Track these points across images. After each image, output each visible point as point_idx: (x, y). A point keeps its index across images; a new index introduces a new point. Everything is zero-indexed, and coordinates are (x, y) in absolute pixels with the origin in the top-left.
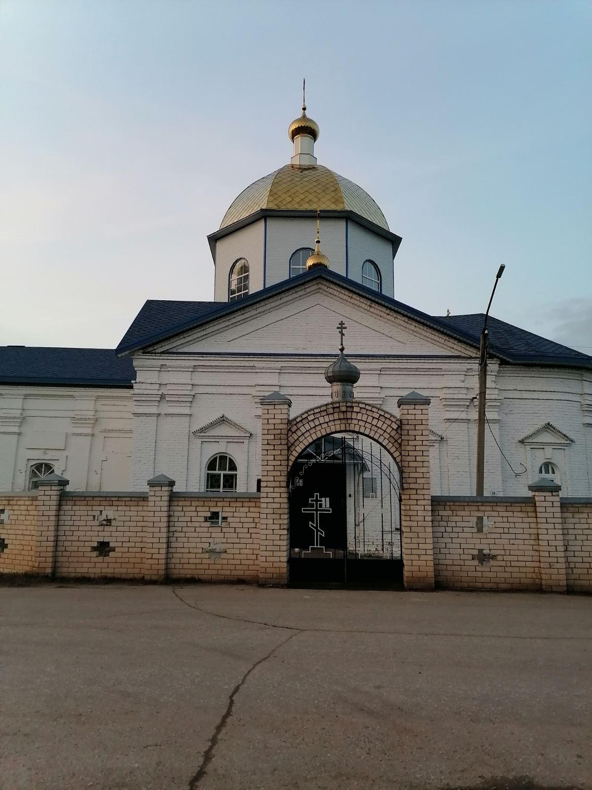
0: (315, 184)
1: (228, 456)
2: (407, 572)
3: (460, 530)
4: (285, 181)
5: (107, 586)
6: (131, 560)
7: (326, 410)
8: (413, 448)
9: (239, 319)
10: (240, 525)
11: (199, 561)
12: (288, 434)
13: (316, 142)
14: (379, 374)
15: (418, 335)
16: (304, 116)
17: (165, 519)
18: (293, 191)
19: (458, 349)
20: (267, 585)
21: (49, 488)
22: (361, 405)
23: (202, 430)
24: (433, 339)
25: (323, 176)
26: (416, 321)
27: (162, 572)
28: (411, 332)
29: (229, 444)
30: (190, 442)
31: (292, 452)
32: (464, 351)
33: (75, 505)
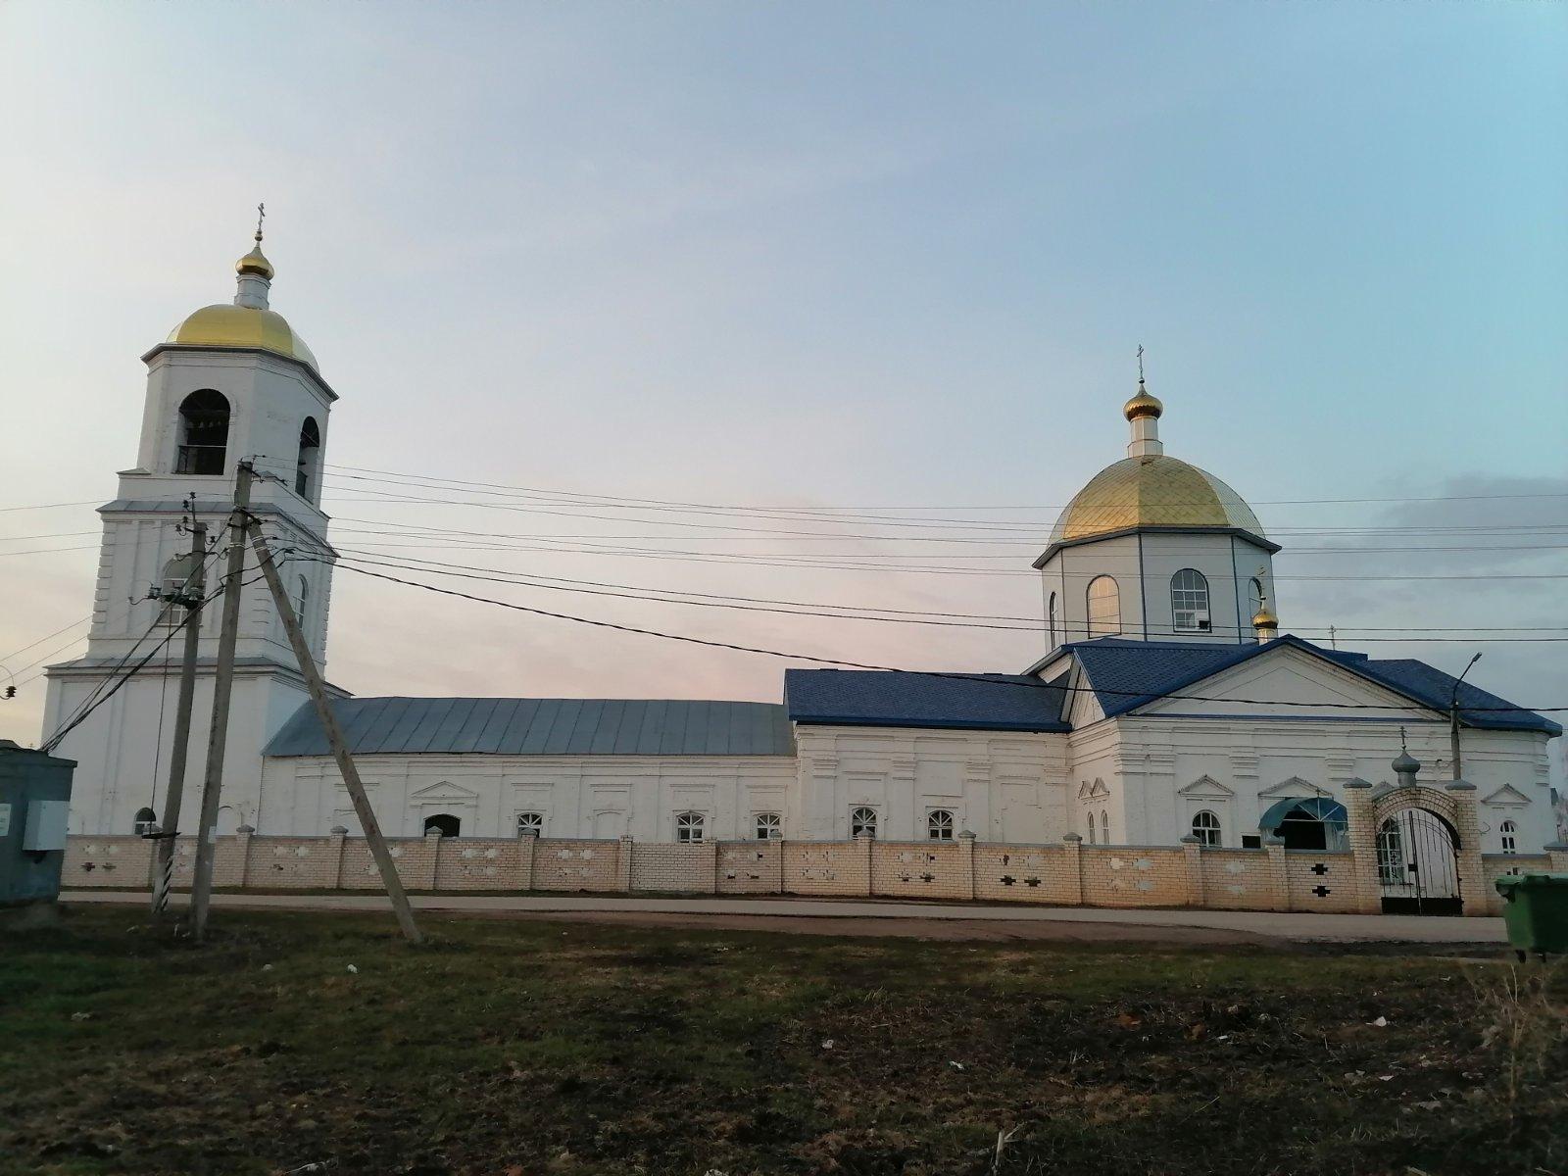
2: (1465, 907)
23: (1188, 789)
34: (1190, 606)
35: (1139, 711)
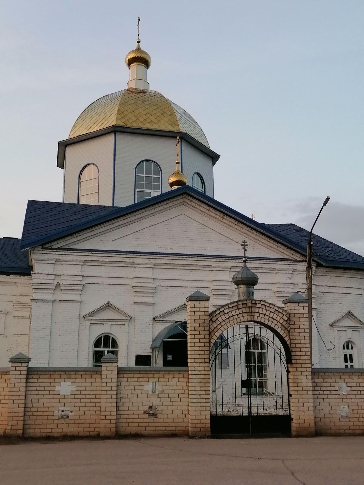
0: (155, 107)
1: (111, 336)
2: (294, 425)
3: (328, 392)
4: (129, 103)
5: (71, 442)
6: (87, 421)
7: (237, 306)
8: (298, 334)
9: (121, 223)
10: (172, 392)
11: (141, 420)
12: (209, 323)
13: (148, 70)
14: (229, 271)
15: (257, 242)
16: (139, 49)
17: (115, 388)
18: (137, 112)
19: (287, 253)
20: (196, 437)
21: (19, 365)
22: (262, 303)
23: (92, 314)
24: (269, 245)
25: (160, 101)
26: (257, 231)
27: (114, 430)
28: (252, 239)
29: (113, 326)
30: (80, 324)
31: (212, 336)
32: (290, 255)
33: (40, 378)
34: (148, 187)
35: (55, 245)
